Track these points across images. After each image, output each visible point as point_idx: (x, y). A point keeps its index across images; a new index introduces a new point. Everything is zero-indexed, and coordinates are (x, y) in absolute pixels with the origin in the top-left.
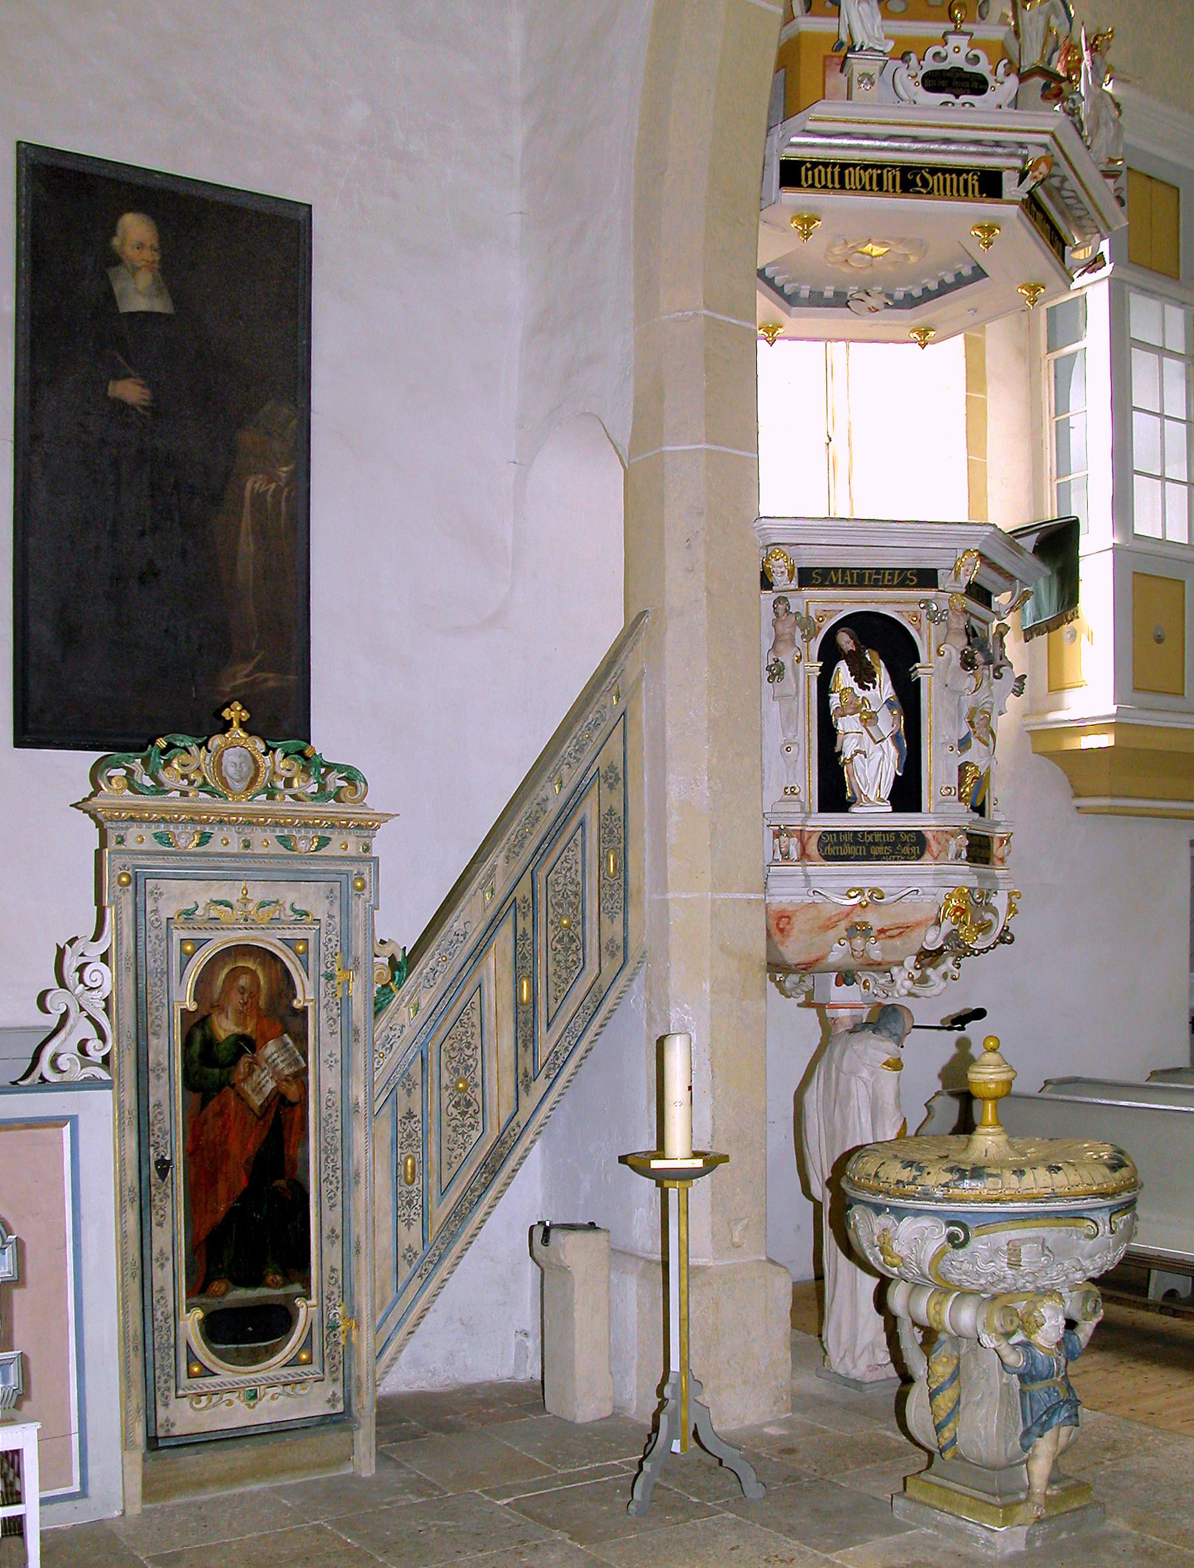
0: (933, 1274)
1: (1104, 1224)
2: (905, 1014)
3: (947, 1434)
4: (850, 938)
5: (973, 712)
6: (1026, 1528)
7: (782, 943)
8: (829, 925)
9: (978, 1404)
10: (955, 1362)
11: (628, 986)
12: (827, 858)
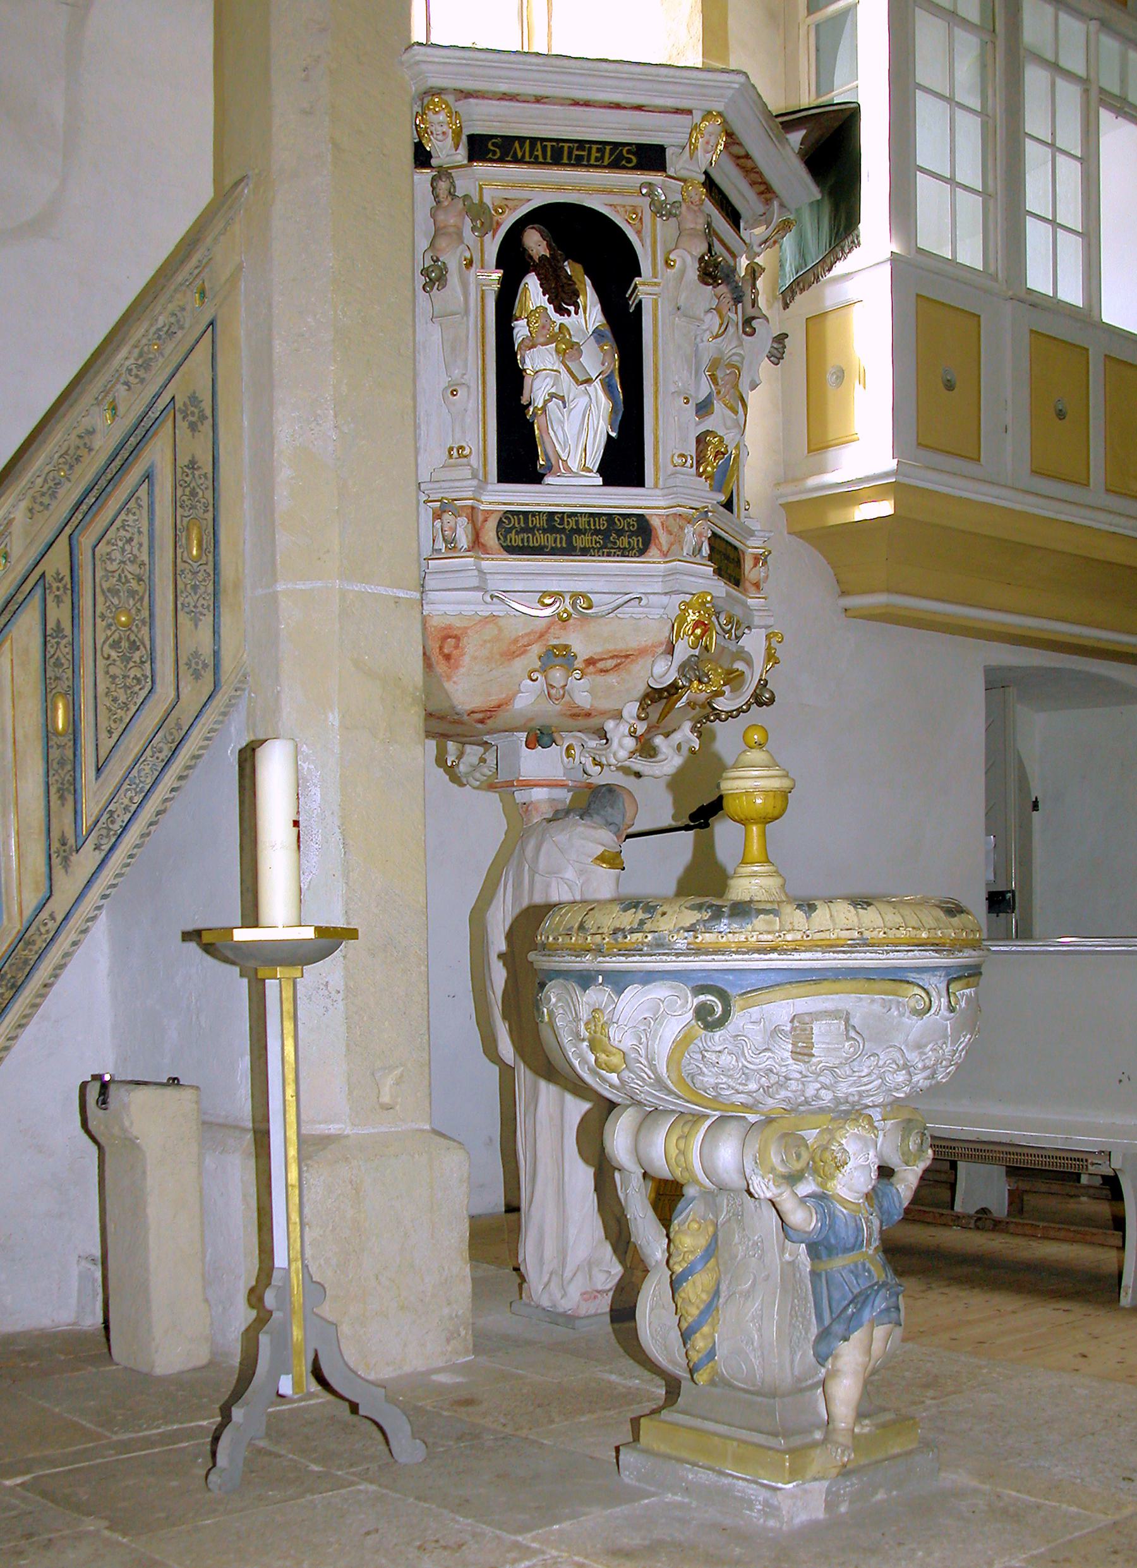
0: (674, 1076)
1: (940, 996)
2: (626, 797)
3: (700, 1343)
4: (544, 670)
5: (715, 364)
6: (826, 1484)
7: (449, 678)
8: (514, 651)
9: (747, 1295)
10: (711, 1229)
11: (221, 722)
12: (511, 550)
